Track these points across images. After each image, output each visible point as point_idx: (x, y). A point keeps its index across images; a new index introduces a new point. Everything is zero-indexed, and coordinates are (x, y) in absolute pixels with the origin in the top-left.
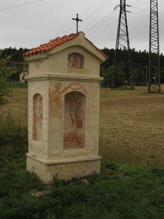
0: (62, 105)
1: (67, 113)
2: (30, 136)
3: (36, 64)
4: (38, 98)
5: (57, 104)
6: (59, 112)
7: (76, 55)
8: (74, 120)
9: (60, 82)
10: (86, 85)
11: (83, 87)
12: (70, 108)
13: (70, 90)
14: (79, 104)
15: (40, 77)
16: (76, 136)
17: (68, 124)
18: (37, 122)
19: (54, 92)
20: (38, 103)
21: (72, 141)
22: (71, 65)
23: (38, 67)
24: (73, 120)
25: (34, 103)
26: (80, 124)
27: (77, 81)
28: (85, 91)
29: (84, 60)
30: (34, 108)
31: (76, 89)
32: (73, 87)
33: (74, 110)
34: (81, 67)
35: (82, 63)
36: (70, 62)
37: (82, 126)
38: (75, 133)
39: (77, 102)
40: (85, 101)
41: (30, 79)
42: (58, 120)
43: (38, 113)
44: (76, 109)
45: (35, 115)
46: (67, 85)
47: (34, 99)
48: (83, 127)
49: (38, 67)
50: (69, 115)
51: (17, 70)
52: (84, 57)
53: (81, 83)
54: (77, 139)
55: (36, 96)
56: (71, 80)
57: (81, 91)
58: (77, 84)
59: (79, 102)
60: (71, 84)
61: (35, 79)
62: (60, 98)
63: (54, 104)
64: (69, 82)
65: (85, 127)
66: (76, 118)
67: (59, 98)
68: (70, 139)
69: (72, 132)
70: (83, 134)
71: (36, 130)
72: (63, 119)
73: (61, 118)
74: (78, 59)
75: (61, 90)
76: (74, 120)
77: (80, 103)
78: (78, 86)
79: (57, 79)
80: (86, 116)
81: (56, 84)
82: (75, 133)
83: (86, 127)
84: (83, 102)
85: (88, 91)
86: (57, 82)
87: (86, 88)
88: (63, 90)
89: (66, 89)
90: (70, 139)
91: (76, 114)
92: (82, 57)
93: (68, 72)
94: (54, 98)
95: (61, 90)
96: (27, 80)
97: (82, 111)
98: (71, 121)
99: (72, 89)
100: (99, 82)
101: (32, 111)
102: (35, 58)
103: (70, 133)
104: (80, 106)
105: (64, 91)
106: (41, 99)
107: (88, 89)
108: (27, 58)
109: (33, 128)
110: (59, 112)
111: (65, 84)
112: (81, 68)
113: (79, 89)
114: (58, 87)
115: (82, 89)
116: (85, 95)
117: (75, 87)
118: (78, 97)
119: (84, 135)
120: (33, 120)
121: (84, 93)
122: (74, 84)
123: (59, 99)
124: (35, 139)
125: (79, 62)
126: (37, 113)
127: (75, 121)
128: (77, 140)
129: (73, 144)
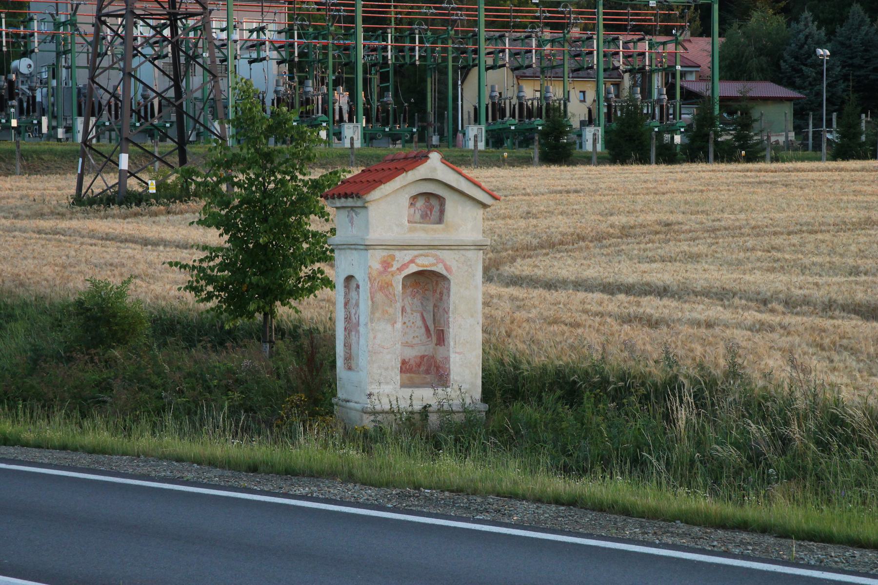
0: (397, 298)
1: (415, 314)
2: (340, 362)
3: (348, 216)
4: (353, 285)
5: (386, 296)
6: (391, 311)
7: (428, 195)
8: (432, 328)
9: (391, 252)
10: (447, 256)
11: (443, 261)
12: (422, 304)
13: (413, 269)
14: (438, 296)
15: (354, 243)
16: (435, 362)
17: (417, 337)
18: (353, 333)
19: (380, 273)
20: (353, 294)
21: (427, 372)
22: (418, 216)
23: (351, 222)
24: (427, 329)
25: (346, 294)
26: (441, 338)
27: (429, 249)
28: (447, 268)
29: (444, 205)
30: (346, 304)
31: (422, 255)
32: (419, 261)
33: (430, 308)
34: (440, 220)
35: (442, 212)
36: (417, 211)
37: (444, 341)
38: (433, 357)
39: (436, 291)
40: (449, 290)
41: (337, 245)
42: (389, 328)
43: (355, 314)
44: (435, 306)
45: (348, 319)
46: (407, 259)
47: (345, 287)
48: (446, 343)
49: (351, 222)
50: (419, 318)
51: (198, 94)
52: (444, 199)
53: (438, 253)
54: (438, 368)
55: (349, 279)
56: (416, 247)
57: (439, 269)
58: (428, 256)
59: (438, 292)
60: (416, 256)
61: (345, 246)
62: (392, 285)
63: (379, 297)
64: (410, 251)
65: (449, 343)
66: (434, 324)
67: (389, 285)
68: (423, 368)
69: (426, 354)
70: (446, 358)
71: (350, 349)
72: (399, 325)
73: (395, 322)
74: (434, 202)
75: (394, 268)
76: (432, 328)
77: (441, 294)
78: (432, 260)
79: (384, 247)
80: (451, 320)
81: (384, 257)
82: (433, 357)
83: (452, 343)
84: (445, 291)
85: (454, 269)
86: (385, 253)
87: (448, 263)
88: (398, 269)
89: (405, 266)
90: (423, 368)
91: (434, 315)
92: (441, 200)
93: (411, 230)
94: (380, 283)
95: (394, 268)
96: (69, 56)
97: (444, 309)
98: (423, 330)
99: (418, 265)
100: (480, 250)
101: (343, 310)
102: (349, 204)
103: (422, 357)
104: (441, 299)
105: (400, 270)
106: (358, 287)
107: (454, 265)
108: (289, 316)
109: (345, 345)
110: (391, 311)
111: (407, 255)
112: (440, 220)
113: (434, 265)
114: (389, 264)
115: (441, 265)
116: (449, 277)
117: (425, 262)
118: (437, 281)
119: (447, 359)
120: (345, 329)
121: (444, 273)
122: (422, 255)
123: (389, 288)
124: (350, 369)
125: (436, 209)
126: (353, 315)
127: (432, 332)
128: (437, 370)
129: (429, 380)
